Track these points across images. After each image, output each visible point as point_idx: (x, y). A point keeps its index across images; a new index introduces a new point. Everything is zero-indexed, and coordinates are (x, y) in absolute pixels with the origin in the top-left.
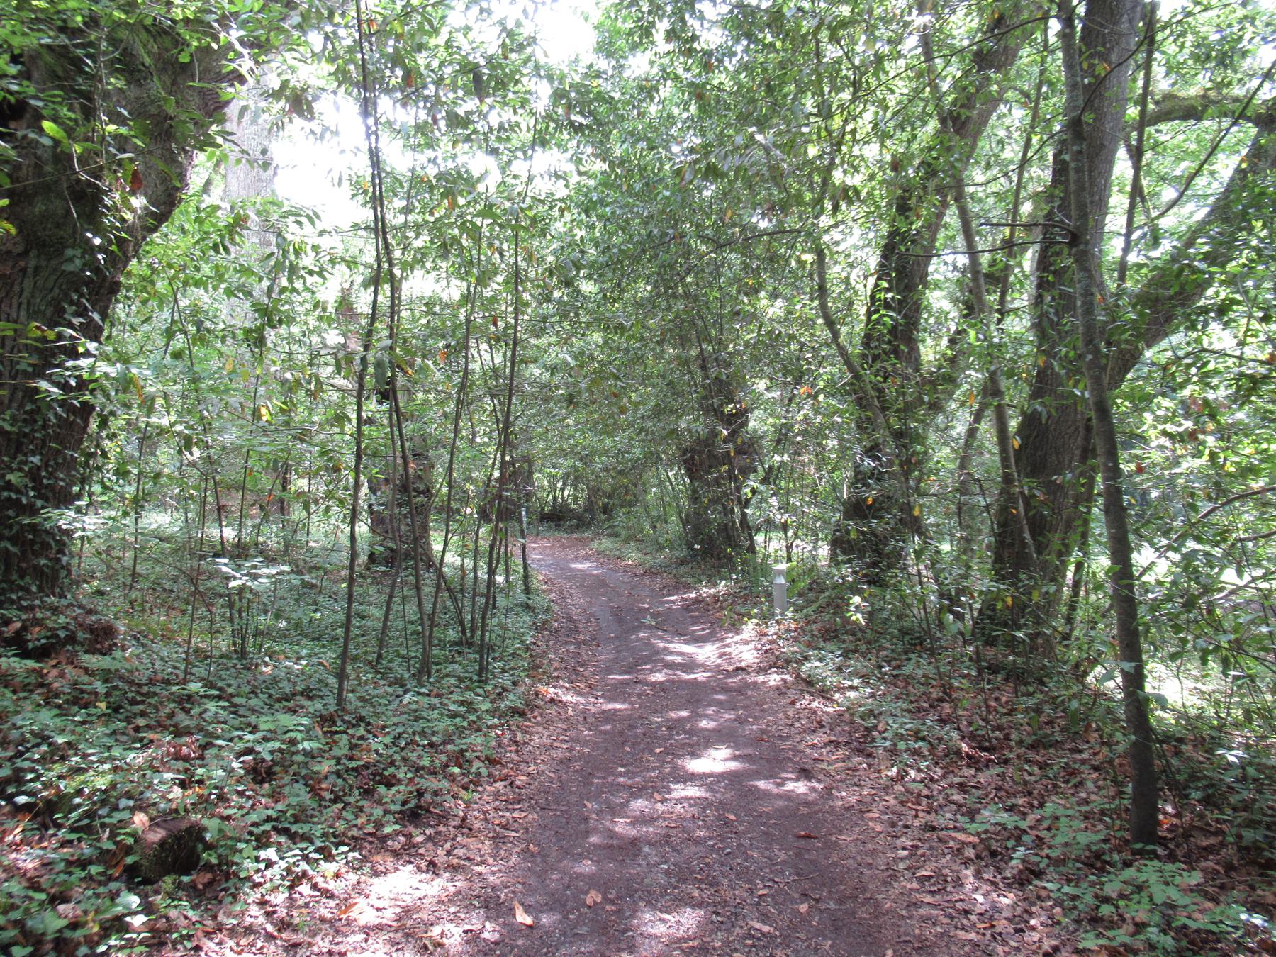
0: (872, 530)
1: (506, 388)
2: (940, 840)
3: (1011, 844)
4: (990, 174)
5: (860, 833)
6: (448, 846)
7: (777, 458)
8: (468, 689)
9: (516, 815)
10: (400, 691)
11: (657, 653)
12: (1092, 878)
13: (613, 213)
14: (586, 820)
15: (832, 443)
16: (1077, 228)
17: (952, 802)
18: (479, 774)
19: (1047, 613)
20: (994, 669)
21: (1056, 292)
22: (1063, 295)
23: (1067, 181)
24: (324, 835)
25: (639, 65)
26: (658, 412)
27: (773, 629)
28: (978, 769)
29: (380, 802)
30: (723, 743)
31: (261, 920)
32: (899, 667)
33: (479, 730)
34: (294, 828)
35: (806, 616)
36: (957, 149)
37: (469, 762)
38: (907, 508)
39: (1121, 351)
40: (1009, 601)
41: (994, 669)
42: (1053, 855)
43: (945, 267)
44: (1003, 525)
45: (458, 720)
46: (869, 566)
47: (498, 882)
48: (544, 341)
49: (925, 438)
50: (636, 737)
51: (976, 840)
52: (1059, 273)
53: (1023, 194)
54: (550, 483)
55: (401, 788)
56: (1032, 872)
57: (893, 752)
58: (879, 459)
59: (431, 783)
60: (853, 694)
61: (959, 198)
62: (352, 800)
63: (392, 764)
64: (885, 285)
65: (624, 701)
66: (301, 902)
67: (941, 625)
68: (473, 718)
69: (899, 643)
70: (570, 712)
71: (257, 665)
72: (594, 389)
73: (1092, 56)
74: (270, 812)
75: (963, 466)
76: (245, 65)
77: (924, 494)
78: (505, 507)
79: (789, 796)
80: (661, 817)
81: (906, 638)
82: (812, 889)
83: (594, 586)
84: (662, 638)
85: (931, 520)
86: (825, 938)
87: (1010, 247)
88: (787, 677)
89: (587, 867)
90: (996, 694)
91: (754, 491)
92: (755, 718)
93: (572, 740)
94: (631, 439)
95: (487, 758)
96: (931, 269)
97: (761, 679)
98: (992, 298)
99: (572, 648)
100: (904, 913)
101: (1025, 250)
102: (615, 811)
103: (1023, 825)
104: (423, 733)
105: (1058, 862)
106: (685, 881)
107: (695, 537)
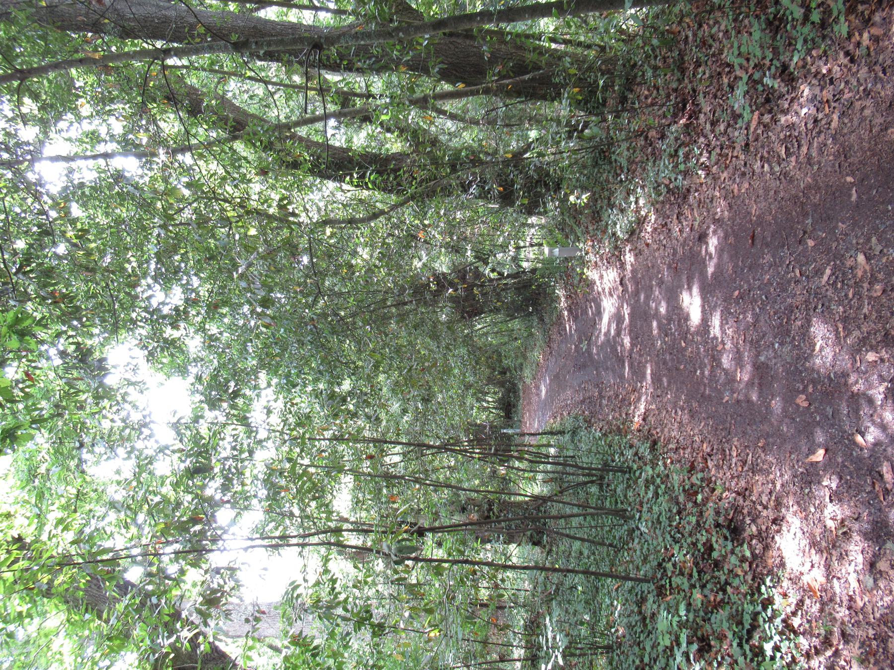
0: (522, 187)
1: (417, 447)
2: (756, 140)
3: (760, 88)
4: (273, 105)
5: (750, 199)
6: (760, 508)
7: (469, 253)
8: (636, 482)
9: (734, 454)
10: (637, 533)
11: (608, 340)
12: (789, 27)
13: (295, 367)
14: (738, 401)
15: (459, 215)
16: (309, 45)
17: (726, 131)
18: (702, 480)
19: (584, 62)
20: (623, 99)
21: (355, 59)
22: (357, 54)
23: (278, 51)
24: (752, 602)
25: (194, 344)
26: (435, 336)
27: (591, 257)
28: (700, 112)
29: (725, 557)
30: (678, 296)
31: (822, 659)
32: (621, 168)
33: (668, 476)
34: (747, 626)
35: (583, 234)
36: (255, 128)
37: (692, 485)
38: (507, 163)
39: (396, 13)
40: (576, 90)
41: (623, 99)
42: (771, 56)
43: (337, 135)
44: (519, 94)
45: (660, 492)
46: (548, 190)
47: (789, 473)
48: (383, 416)
49: (456, 148)
50: (673, 360)
51: (757, 113)
52: (342, 57)
53: (287, 82)
54: (484, 411)
55: (714, 539)
56: (783, 72)
57: (686, 173)
58: (471, 182)
59: (709, 514)
60: (641, 202)
61: (288, 127)
62: (723, 578)
63: (694, 544)
64: (348, 178)
65: (645, 367)
66: (807, 626)
67: (591, 138)
68: (658, 481)
69: (603, 168)
70: (653, 407)
71: (617, 637)
72: (417, 383)
73: (193, 37)
74: (735, 644)
75: (477, 123)
76: (186, 634)
77: (496, 152)
78: (497, 444)
79: (720, 250)
80: (736, 345)
81: (600, 162)
82: (795, 235)
83: (558, 382)
84: (598, 337)
85: (514, 144)
86: (836, 227)
87: (323, 91)
88: (628, 249)
89: (776, 404)
90: (642, 98)
91: (493, 270)
92: (659, 272)
93: (675, 407)
94: (454, 356)
95: (689, 472)
96: (337, 144)
97: (629, 267)
98: (359, 102)
99: (604, 402)
100: (816, 167)
101: (325, 80)
102: (731, 380)
103: (745, 78)
104: (670, 519)
105: (776, 52)
106: (788, 332)
107: (524, 311)
